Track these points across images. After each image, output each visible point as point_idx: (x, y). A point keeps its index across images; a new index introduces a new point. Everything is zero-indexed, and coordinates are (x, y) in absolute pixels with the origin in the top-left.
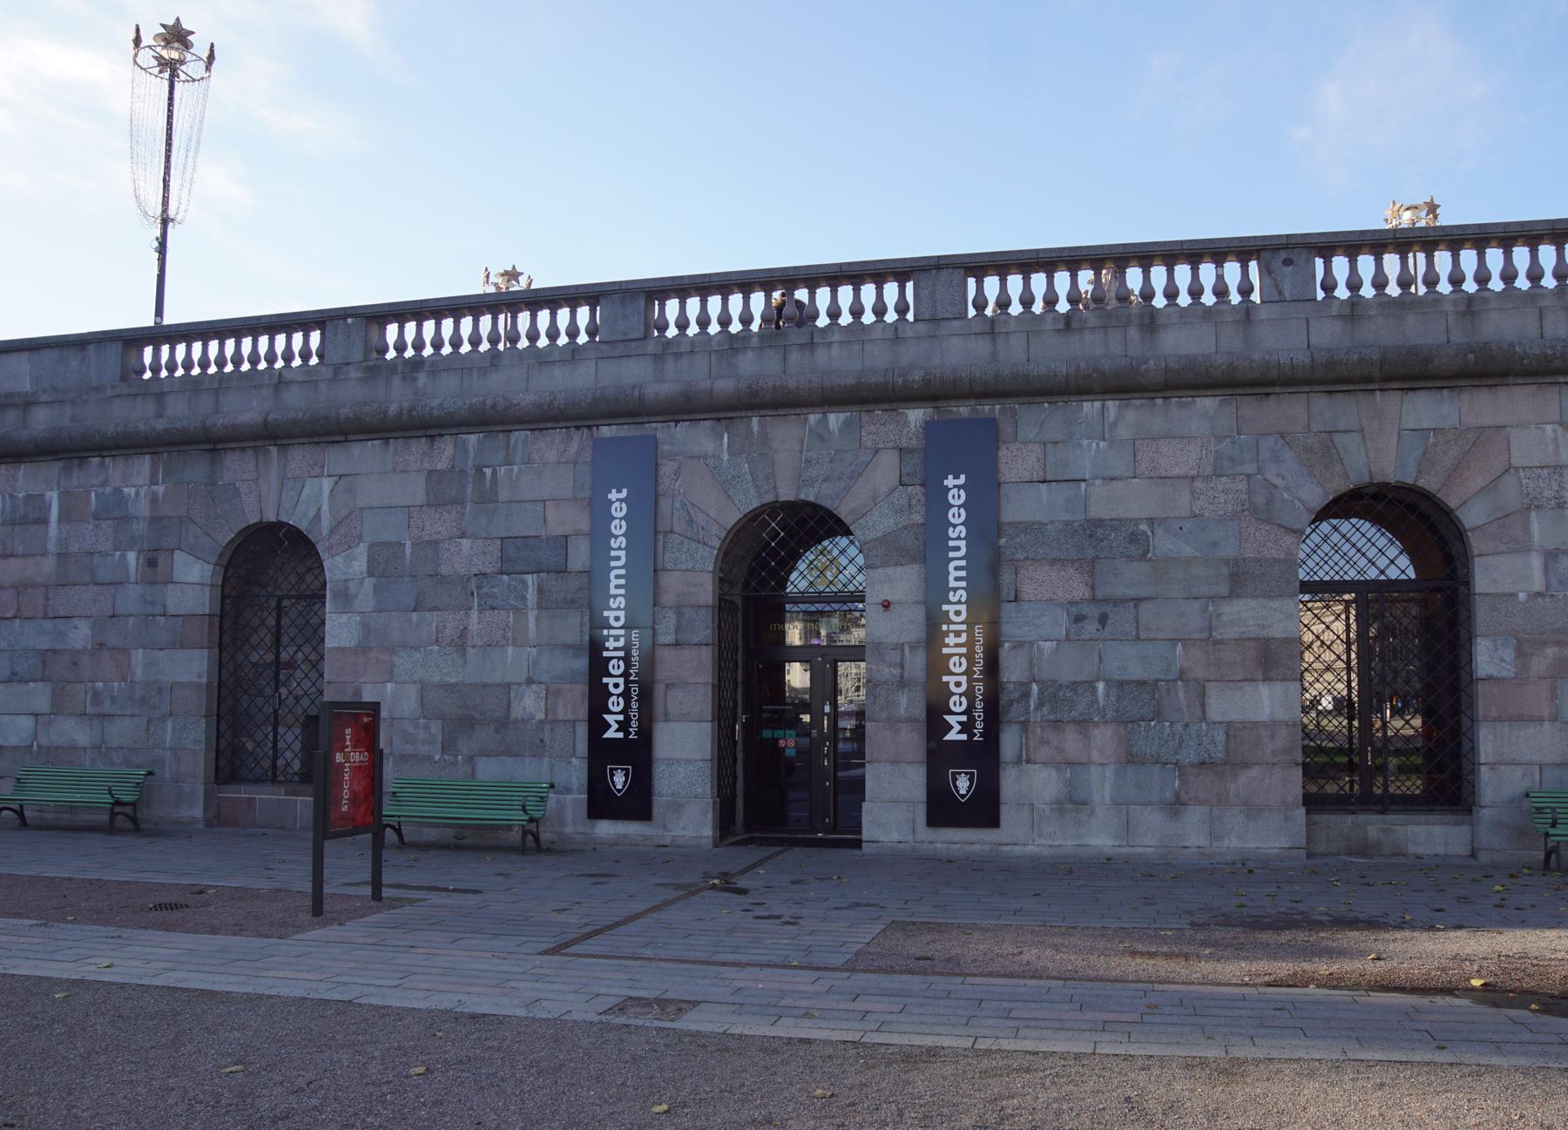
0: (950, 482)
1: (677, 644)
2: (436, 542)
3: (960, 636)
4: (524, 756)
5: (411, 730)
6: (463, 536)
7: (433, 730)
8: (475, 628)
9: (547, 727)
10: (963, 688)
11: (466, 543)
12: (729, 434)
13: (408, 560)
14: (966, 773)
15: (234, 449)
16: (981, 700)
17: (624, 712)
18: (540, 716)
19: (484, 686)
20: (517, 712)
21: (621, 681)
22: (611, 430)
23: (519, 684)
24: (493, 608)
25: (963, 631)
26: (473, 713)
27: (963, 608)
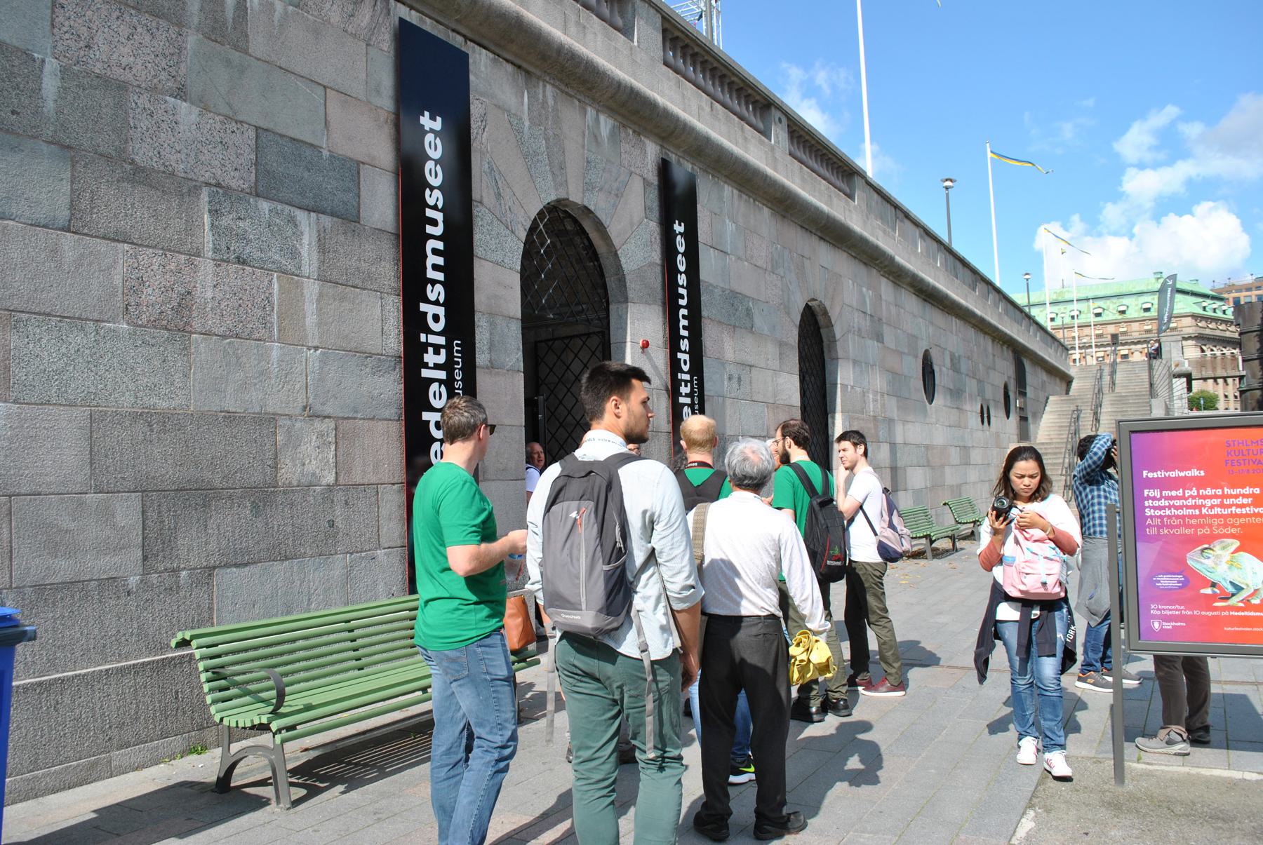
0: (425, 120)
2: (123, 87)
4: (304, 556)
5: (65, 522)
6: (181, 93)
7: (121, 520)
8: (209, 295)
9: (339, 496)
11: (187, 112)
12: (528, 92)
13: (50, 104)
15: (828, 241)
18: (330, 478)
19: (231, 418)
20: (289, 472)
22: (421, 20)
24: (241, 261)
26: (207, 475)
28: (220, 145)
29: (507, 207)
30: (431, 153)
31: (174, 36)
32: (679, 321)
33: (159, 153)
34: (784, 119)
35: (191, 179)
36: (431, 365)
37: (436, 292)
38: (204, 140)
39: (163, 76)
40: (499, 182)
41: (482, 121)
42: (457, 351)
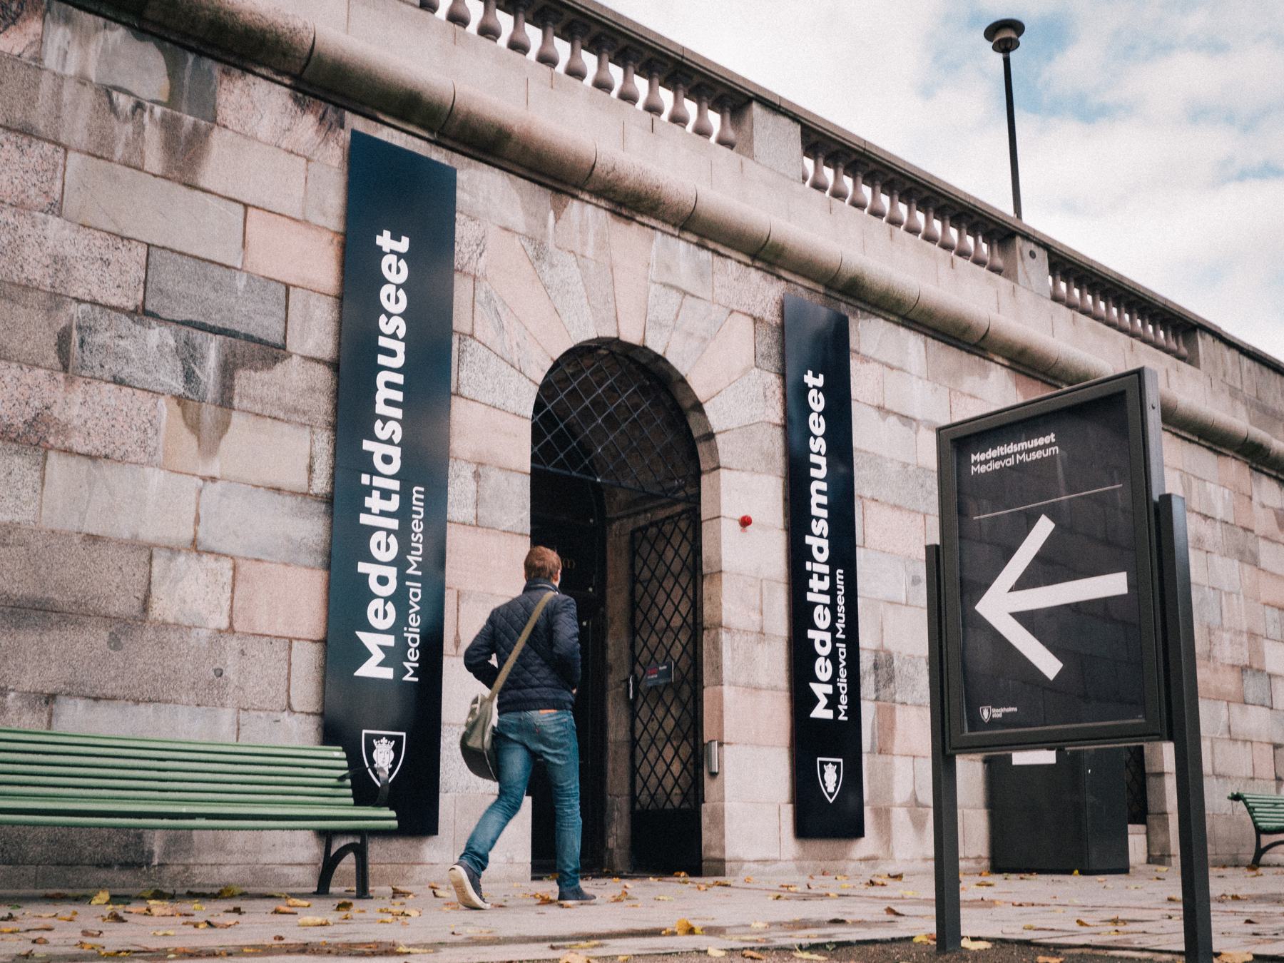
0: (384, 240)
1: (477, 524)
3: (389, 499)
6: (56, 208)
10: (391, 588)
14: (390, 738)
16: (416, 613)
17: (396, 630)
21: (391, 573)
23: (173, 551)
24: (118, 381)
25: (395, 492)
27: (396, 453)
28: (100, 262)
29: (514, 344)
30: (813, 405)
31: (49, 153)
32: (811, 496)
33: (21, 267)
34: (1042, 254)
35: (60, 294)
36: (816, 590)
37: (820, 527)
38: (79, 255)
39: (33, 191)
40: (503, 315)
41: (478, 245)
42: (417, 499)
